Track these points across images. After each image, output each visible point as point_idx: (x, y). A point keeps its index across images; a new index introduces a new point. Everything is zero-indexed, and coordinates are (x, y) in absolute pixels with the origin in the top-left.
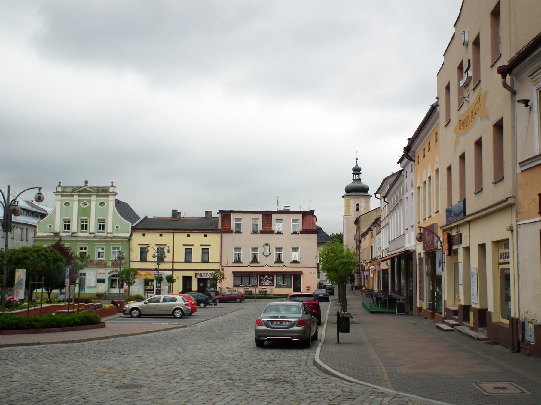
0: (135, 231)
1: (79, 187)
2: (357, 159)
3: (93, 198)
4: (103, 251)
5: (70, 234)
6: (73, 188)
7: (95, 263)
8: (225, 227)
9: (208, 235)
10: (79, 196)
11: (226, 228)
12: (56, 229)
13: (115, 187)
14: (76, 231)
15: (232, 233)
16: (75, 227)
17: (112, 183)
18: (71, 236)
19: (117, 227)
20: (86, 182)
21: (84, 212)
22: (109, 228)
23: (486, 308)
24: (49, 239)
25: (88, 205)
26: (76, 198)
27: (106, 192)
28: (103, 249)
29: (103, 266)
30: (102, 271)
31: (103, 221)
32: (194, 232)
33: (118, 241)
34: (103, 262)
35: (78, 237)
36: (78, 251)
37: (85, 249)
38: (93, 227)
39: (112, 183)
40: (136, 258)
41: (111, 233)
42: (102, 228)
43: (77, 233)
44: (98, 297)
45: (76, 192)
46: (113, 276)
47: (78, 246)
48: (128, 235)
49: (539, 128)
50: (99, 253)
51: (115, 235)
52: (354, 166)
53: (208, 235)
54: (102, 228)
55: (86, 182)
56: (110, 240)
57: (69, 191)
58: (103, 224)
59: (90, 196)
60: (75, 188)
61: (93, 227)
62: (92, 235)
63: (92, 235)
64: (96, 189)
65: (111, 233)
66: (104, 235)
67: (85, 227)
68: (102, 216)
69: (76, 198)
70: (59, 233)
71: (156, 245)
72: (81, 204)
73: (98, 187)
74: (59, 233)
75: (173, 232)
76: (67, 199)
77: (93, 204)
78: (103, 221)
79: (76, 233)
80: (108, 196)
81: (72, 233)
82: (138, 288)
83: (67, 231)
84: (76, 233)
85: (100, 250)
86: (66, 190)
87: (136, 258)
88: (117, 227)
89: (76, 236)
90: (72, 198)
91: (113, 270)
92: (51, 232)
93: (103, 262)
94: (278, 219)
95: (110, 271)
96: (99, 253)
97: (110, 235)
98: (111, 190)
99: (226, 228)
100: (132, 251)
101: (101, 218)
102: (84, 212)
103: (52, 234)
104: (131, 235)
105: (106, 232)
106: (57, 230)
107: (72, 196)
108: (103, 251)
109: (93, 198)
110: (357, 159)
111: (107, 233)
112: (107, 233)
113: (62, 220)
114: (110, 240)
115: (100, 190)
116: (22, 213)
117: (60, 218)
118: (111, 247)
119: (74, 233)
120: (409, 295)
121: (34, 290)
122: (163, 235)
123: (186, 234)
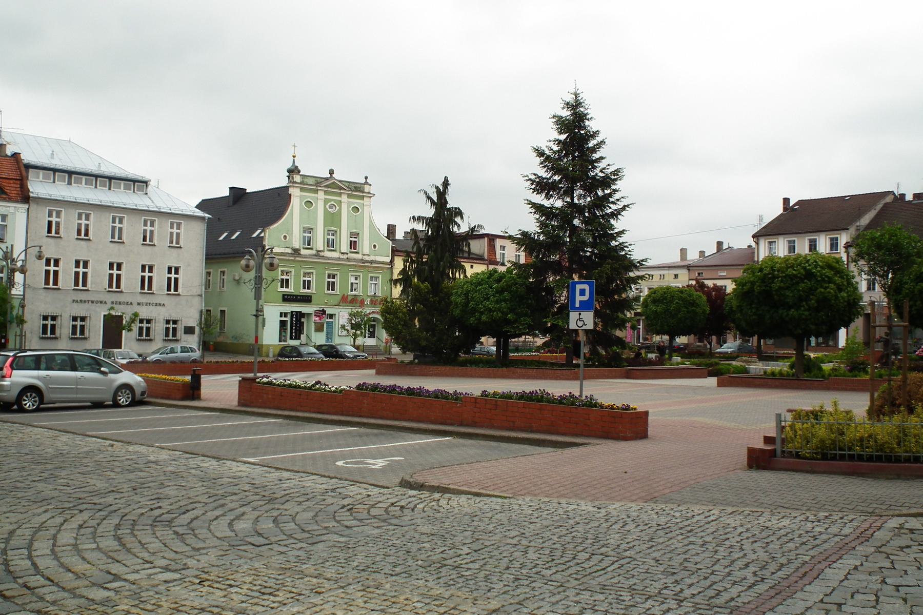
0: (396, 253)
1: (324, 178)
2: (294, 157)
3: (344, 198)
4: (356, 281)
5: (314, 252)
6: (316, 179)
7: (349, 299)
10: (326, 193)
12: (294, 243)
13: (370, 185)
14: (322, 249)
17: (366, 178)
18: (316, 255)
19: (375, 246)
20: (331, 172)
21: (332, 219)
24: (288, 258)
25: (327, 207)
26: (321, 195)
27: (360, 191)
28: (356, 279)
31: (310, 230)
32: (478, 262)
33: (378, 267)
34: (359, 299)
36: (90, 269)
37: (333, 278)
39: (366, 178)
43: (323, 251)
45: (325, 186)
48: (388, 260)
51: (372, 258)
52: (289, 165)
54: (353, 245)
55: (331, 172)
56: (369, 265)
57: (311, 183)
58: (355, 240)
59: (340, 195)
60: (319, 179)
62: (345, 257)
63: (345, 257)
64: (347, 184)
66: (359, 256)
68: (356, 229)
69: (321, 195)
72: (327, 207)
73: (350, 182)
76: (309, 196)
77: (345, 209)
78: (310, 230)
80: (362, 198)
81: (318, 251)
83: (353, 250)
85: (352, 280)
86: (306, 180)
88: (375, 246)
89: (323, 256)
90: (316, 195)
92: (287, 248)
93: (359, 299)
97: (366, 258)
98: (367, 188)
101: (354, 230)
102: (332, 219)
103: (289, 251)
105: (360, 252)
106: (297, 244)
107: (316, 191)
108: (356, 281)
109: (344, 198)
110: (294, 157)
111: (364, 255)
112: (364, 255)
113: (349, 233)
114: (369, 265)
115: (352, 186)
116: (866, 258)
117: (300, 227)
118: (370, 275)
119: (321, 251)
121: (771, 339)
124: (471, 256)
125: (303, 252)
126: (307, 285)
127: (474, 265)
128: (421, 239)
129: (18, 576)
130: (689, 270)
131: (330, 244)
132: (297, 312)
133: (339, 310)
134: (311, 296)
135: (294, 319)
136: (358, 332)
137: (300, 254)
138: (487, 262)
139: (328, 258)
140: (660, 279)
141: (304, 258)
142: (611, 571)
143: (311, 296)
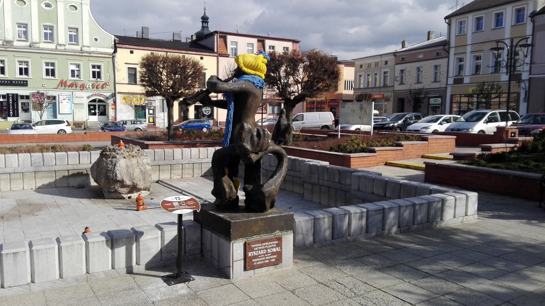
7: (68, 84)
8: (221, 50)
9: (135, 51)
11: (222, 51)
14: (38, 41)
15: (228, 57)
16: (36, 34)
22: (86, 39)
23: (446, 113)
29: (78, 88)
30: (78, 93)
35: (38, 48)
38: (62, 36)
40: (123, 79)
41: (88, 47)
42: (74, 38)
44: (76, 127)
46: (94, 101)
47: (43, 61)
49: (471, 60)
50: (73, 71)
51: (92, 49)
53: (135, 51)
54: (74, 38)
61: (62, 36)
65: (88, 47)
67: (50, 36)
70: (12, 42)
71: (126, 63)
74: (12, 42)
75: (167, 51)
79: (38, 43)
82: (127, 115)
84: (38, 43)
85: (73, 67)
87: (123, 79)
91: (94, 93)
94: (233, 42)
95: (90, 94)
96: (73, 71)
99: (222, 51)
100: (118, 71)
101: (48, 24)
104: (115, 51)
106: (9, 37)
110: (205, 9)
120: (495, 83)
122: (204, 58)
123: (129, 50)
124: (459, 96)
125: (16, 44)
126: (24, 71)
127: (134, 51)
128: (398, 81)
129: (160, 258)
130: (395, 56)
131: (50, 36)
132: (13, 95)
133: (59, 93)
134: (27, 81)
135: (11, 100)
136: (260, 124)
137: (12, 45)
138: (216, 55)
139: (42, 49)
140: (376, 66)
141: (15, 48)
142: (476, 262)
143: (27, 81)
